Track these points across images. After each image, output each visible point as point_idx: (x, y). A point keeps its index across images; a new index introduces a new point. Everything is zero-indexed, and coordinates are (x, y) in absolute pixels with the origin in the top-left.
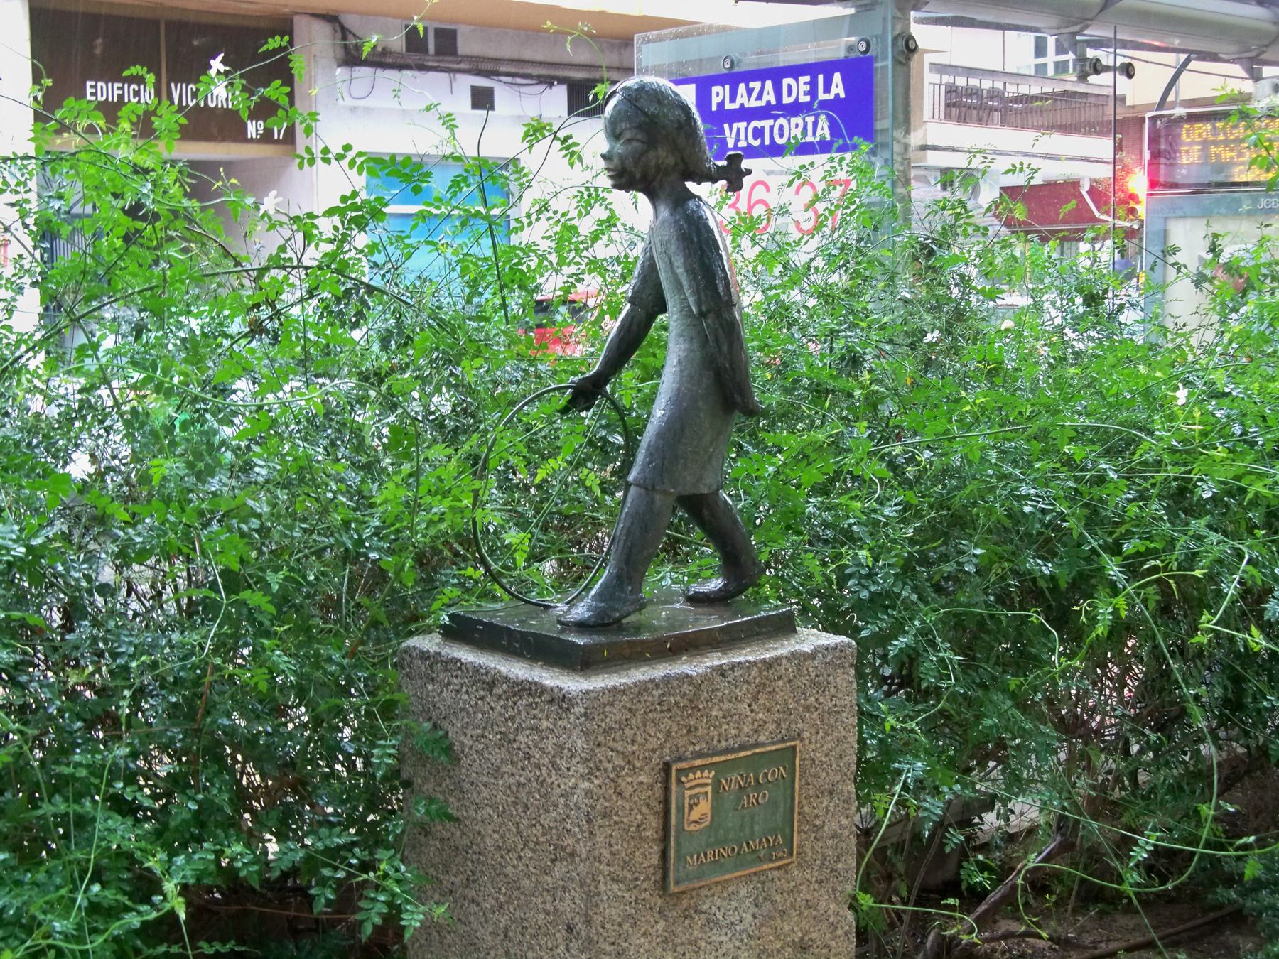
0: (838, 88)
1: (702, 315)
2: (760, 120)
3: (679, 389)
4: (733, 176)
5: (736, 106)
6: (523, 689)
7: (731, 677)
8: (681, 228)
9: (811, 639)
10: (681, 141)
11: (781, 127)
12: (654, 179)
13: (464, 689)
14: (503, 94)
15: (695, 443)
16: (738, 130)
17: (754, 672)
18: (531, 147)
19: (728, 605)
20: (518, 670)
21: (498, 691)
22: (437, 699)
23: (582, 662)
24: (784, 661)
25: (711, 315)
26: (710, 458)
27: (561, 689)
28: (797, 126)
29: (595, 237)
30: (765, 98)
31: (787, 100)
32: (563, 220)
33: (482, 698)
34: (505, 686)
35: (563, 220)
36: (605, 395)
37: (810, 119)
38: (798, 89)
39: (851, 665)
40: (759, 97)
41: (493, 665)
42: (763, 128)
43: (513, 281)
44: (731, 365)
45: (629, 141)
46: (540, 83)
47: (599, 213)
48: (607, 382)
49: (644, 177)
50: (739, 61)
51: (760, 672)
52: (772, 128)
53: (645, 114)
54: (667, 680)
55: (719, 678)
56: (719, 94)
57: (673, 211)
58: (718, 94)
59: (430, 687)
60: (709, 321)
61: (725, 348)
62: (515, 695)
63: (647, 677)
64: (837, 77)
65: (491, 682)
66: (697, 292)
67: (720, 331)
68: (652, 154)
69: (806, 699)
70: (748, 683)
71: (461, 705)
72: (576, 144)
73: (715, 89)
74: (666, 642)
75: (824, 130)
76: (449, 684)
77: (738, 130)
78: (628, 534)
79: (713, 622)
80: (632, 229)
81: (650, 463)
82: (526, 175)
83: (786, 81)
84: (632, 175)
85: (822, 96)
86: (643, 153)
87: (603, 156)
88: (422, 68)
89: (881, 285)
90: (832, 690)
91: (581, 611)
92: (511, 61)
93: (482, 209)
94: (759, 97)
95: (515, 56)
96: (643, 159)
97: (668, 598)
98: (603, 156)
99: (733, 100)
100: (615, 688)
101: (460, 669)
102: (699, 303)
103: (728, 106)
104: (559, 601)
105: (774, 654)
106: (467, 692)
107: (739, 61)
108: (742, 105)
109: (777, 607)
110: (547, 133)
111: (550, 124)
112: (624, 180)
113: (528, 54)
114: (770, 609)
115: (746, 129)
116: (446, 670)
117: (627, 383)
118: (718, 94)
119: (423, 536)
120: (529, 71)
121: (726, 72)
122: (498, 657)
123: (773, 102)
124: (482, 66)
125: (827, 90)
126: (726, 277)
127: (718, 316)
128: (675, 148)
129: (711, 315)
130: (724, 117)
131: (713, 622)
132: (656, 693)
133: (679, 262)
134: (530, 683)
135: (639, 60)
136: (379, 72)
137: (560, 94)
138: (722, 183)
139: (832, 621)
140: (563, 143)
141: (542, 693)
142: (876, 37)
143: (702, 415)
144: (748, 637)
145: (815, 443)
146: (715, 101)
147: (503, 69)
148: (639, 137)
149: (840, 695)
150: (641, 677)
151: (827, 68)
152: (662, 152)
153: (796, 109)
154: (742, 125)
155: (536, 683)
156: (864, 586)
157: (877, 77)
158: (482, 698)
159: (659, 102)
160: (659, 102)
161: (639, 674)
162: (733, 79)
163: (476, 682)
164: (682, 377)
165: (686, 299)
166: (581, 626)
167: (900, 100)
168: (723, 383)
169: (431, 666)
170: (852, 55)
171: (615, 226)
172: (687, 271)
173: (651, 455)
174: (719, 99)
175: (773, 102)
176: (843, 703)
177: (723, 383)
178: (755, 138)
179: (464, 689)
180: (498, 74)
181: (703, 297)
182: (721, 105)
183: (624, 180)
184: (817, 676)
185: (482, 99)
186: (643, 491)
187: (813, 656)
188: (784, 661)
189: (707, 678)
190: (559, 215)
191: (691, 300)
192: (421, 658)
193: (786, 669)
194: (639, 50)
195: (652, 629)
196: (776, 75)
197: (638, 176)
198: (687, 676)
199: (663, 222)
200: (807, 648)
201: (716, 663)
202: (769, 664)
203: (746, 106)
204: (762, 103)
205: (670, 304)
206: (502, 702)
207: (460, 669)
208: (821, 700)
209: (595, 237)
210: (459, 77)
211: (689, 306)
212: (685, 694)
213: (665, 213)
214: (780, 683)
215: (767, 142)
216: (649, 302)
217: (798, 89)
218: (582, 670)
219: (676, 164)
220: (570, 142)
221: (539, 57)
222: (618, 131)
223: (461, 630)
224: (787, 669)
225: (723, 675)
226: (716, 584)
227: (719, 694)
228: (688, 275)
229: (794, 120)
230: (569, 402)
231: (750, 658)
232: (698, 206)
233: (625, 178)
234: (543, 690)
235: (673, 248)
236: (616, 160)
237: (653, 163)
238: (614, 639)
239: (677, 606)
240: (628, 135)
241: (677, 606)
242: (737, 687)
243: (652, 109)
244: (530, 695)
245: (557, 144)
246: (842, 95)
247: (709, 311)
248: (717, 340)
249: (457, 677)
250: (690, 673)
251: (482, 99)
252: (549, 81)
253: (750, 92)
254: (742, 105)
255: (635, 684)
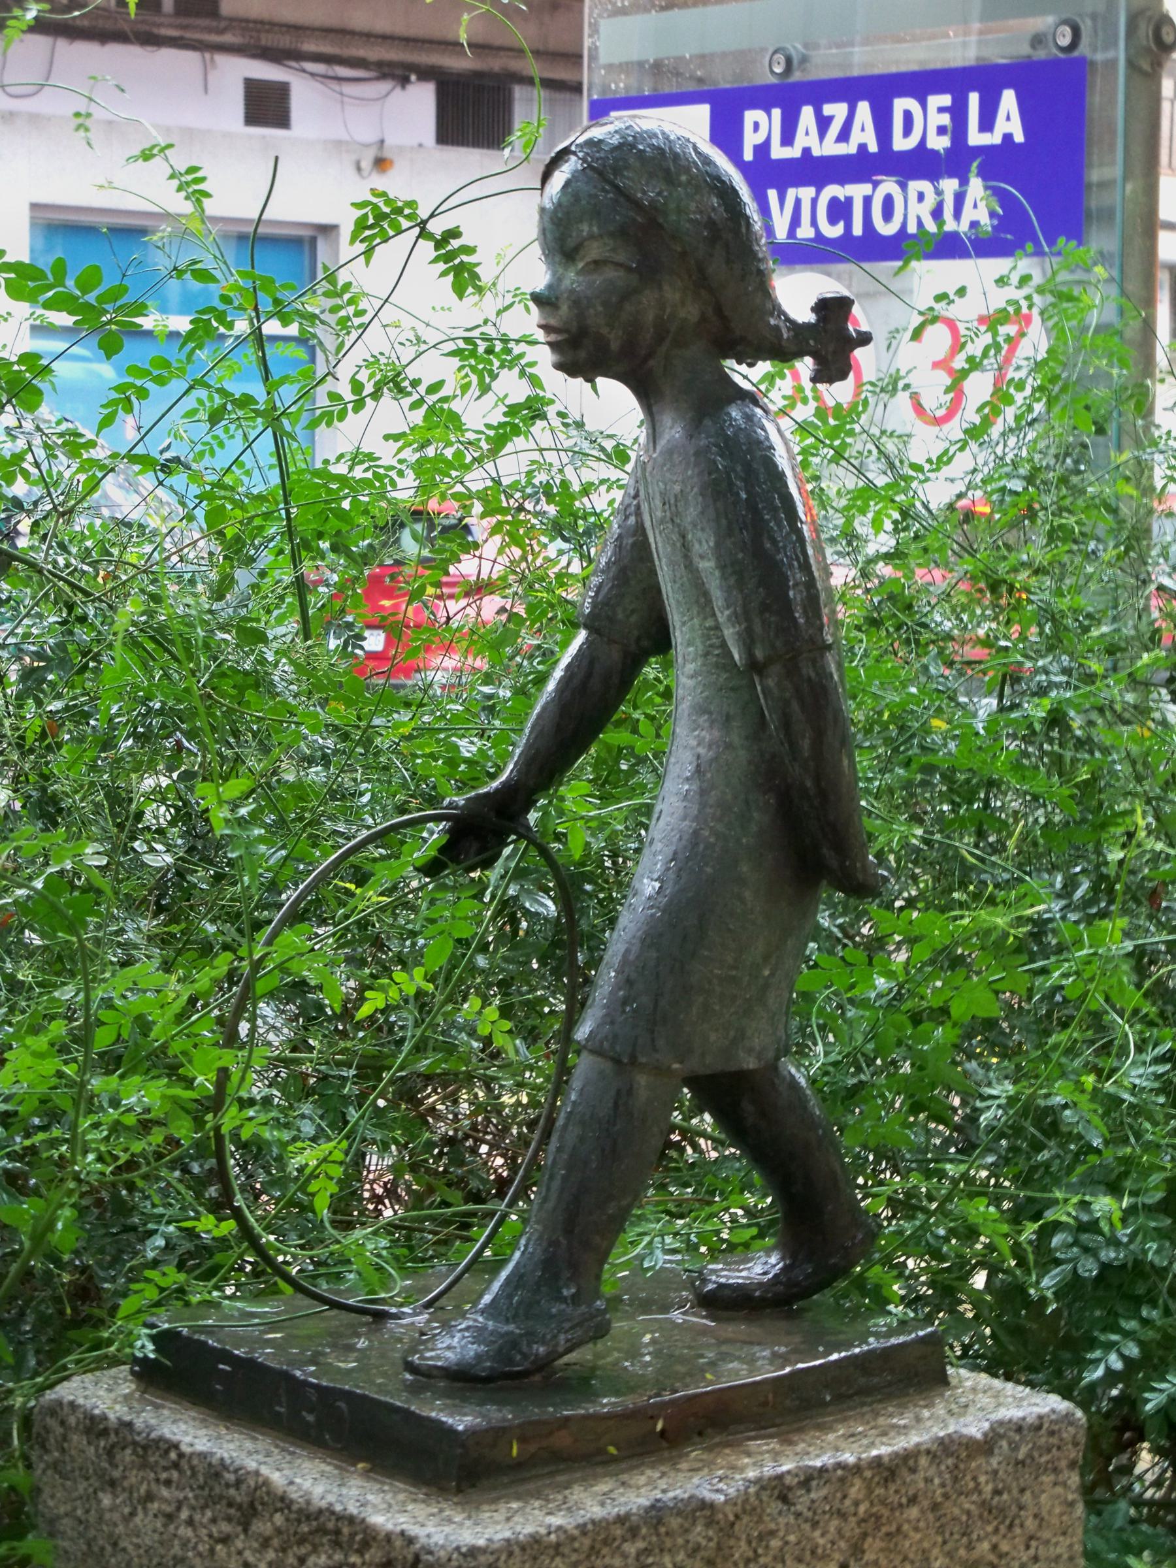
0: (1010, 120)
1: (755, 667)
2: (842, 182)
3: (696, 833)
4: (831, 341)
5: (794, 152)
6: (322, 1530)
7: (802, 1502)
8: (712, 468)
9: (986, 1404)
10: (717, 268)
11: (888, 202)
12: (651, 355)
13: (184, 1514)
14: (306, 94)
15: (730, 959)
16: (798, 202)
17: (856, 1489)
18: (368, 253)
19: (791, 1316)
20: (312, 1480)
21: (261, 1527)
22: (120, 1529)
23: (458, 1471)
24: (923, 1461)
25: (776, 669)
26: (766, 986)
27: (411, 1541)
28: (921, 197)
29: (501, 437)
30: (856, 138)
31: (901, 143)
32: (431, 399)
33: (225, 1540)
34: (279, 1519)
35: (431, 399)
36: (525, 833)
37: (950, 185)
38: (925, 122)
39: (1072, 1465)
40: (844, 136)
41: (251, 1465)
42: (849, 200)
43: (320, 536)
44: (817, 779)
45: (597, 264)
46: (383, 77)
47: (512, 387)
48: (530, 804)
49: (629, 348)
50: (804, 60)
51: (870, 1491)
52: (867, 201)
53: (637, 204)
54: (656, 1514)
55: (775, 1506)
56: (759, 126)
57: (695, 426)
58: (756, 126)
59: (106, 1500)
60: (771, 682)
61: (806, 744)
62: (302, 1541)
63: (612, 1511)
64: (1009, 100)
65: (251, 1503)
66: (743, 616)
67: (795, 706)
68: (648, 298)
69: (970, 1547)
70: (842, 1515)
71: (176, 1550)
72: (469, 250)
73: (751, 116)
74: (653, 1418)
75: (978, 206)
76: (150, 1497)
77: (798, 202)
78: (570, 1167)
79: (756, 1362)
80: (580, 425)
81: (625, 1002)
82: (351, 302)
83: (901, 105)
84: (601, 345)
85: (976, 138)
86: (627, 295)
87: (537, 298)
88: (150, 39)
89: (1108, 554)
90: (1031, 1524)
91: (452, 1347)
92: (327, 32)
93: (258, 390)
94: (844, 136)
95: (333, 21)
96: (628, 307)
97: (653, 1296)
98: (537, 298)
99: (788, 138)
100: (535, 1539)
101: (176, 1465)
102: (748, 640)
103: (778, 152)
104: (409, 1296)
105: (902, 1443)
106: (190, 1522)
107: (804, 60)
108: (807, 151)
109: (904, 1325)
110: (405, 224)
111: (411, 204)
112: (582, 354)
113: (360, 20)
114: (888, 1329)
115: (814, 202)
116: (144, 1465)
117: (575, 809)
118: (756, 126)
119: (100, 1159)
120: (361, 53)
121: (773, 80)
122: (264, 1443)
123: (873, 148)
124: (266, 40)
125: (987, 124)
126: (811, 583)
127: (792, 670)
128: (701, 281)
129: (776, 669)
130: (768, 173)
131: (756, 1362)
132: (631, 1548)
133: (703, 544)
134: (340, 1517)
135: (594, 50)
136: (62, 44)
137: (418, 104)
138: (806, 366)
139: (1027, 1346)
140: (439, 245)
141: (365, 1545)
142: (1094, 17)
143: (747, 894)
144: (839, 1398)
145: (988, 932)
146: (751, 140)
147: (310, 47)
148: (621, 257)
149: (1046, 1534)
150: (596, 1511)
151: (986, 80)
152: (672, 293)
153: (921, 164)
154: (806, 193)
155: (351, 1520)
156: (1086, 1250)
157: (1095, 99)
158: (225, 1540)
159: (669, 178)
160: (669, 178)
161: (595, 1502)
162: (790, 97)
163: (212, 1500)
164: (703, 805)
165: (717, 627)
166: (462, 1381)
167: (1138, 150)
168: (798, 826)
169: (110, 1452)
170: (1041, 54)
171: (543, 417)
172: (722, 567)
173: (629, 982)
174: (760, 138)
175: (873, 148)
176: (1053, 1552)
177: (798, 826)
178: (832, 220)
179: (184, 1514)
180: (299, 56)
181: (758, 628)
182: (763, 149)
183: (582, 354)
184: (997, 1492)
185: (266, 107)
186: (607, 1066)
187: (986, 1446)
188: (923, 1461)
189: (746, 1507)
190: (422, 389)
191: (729, 633)
192: (88, 1431)
193: (928, 1480)
194: (595, 30)
195: (619, 1384)
196: (880, 91)
197: (615, 346)
198: (704, 1505)
199: (669, 452)
200: (974, 1428)
201: (768, 1470)
202: (887, 1471)
203: (816, 153)
204: (850, 148)
205: (680, 635)
206: (271, 1555)
207: (176, 1465)
208: (1004, 1547)
209: (501, 437)
210: (222, 59)
211: (724, 645)
212: (697, 1548)
213: (673, 431)
214: (914, 1512)
215: (858, 230)
216: (628, 632)
217: (925, 122)
218: (459, 1491)
219: (703, 319)
220: (455, 243)
221: (382, 25)
222: (571, 243)
223: (185, 1370)
224: (929, 1479)
225: (784, 1499)
226: (762, 1266)
227: (775, 1543)
228: (724, 577)
229: (915, 186)
230: (442, 850)
231: (849, 1458)
232: (749, 418)
233: (581, 353)
234: (368, 1537)
235: (691, 513)
236: (564, 309)
237: (650, 316)
238: (535, 1412)
239: (677, 1316)
240: (594, 251)
241: (677, 1316)
242: (815, 1525)
243: (650, 192)
244: (337, 1544)
245: (426, 249)
246: (1019, 138)
247: (769, 661)
248: (786, 724)
249: (168, 1483)
250: (708, 1495)
251: (266, 107)
252: (399, 74)
253: (823, 123)
254: (807, 151)
255: (582, 1528)
